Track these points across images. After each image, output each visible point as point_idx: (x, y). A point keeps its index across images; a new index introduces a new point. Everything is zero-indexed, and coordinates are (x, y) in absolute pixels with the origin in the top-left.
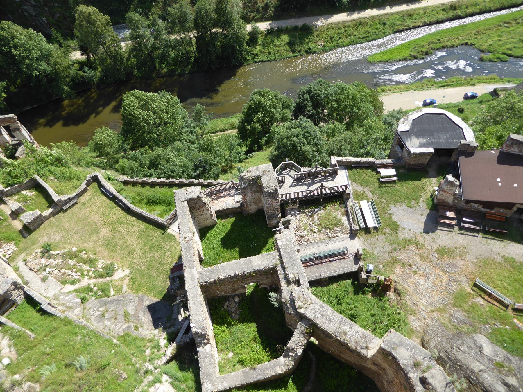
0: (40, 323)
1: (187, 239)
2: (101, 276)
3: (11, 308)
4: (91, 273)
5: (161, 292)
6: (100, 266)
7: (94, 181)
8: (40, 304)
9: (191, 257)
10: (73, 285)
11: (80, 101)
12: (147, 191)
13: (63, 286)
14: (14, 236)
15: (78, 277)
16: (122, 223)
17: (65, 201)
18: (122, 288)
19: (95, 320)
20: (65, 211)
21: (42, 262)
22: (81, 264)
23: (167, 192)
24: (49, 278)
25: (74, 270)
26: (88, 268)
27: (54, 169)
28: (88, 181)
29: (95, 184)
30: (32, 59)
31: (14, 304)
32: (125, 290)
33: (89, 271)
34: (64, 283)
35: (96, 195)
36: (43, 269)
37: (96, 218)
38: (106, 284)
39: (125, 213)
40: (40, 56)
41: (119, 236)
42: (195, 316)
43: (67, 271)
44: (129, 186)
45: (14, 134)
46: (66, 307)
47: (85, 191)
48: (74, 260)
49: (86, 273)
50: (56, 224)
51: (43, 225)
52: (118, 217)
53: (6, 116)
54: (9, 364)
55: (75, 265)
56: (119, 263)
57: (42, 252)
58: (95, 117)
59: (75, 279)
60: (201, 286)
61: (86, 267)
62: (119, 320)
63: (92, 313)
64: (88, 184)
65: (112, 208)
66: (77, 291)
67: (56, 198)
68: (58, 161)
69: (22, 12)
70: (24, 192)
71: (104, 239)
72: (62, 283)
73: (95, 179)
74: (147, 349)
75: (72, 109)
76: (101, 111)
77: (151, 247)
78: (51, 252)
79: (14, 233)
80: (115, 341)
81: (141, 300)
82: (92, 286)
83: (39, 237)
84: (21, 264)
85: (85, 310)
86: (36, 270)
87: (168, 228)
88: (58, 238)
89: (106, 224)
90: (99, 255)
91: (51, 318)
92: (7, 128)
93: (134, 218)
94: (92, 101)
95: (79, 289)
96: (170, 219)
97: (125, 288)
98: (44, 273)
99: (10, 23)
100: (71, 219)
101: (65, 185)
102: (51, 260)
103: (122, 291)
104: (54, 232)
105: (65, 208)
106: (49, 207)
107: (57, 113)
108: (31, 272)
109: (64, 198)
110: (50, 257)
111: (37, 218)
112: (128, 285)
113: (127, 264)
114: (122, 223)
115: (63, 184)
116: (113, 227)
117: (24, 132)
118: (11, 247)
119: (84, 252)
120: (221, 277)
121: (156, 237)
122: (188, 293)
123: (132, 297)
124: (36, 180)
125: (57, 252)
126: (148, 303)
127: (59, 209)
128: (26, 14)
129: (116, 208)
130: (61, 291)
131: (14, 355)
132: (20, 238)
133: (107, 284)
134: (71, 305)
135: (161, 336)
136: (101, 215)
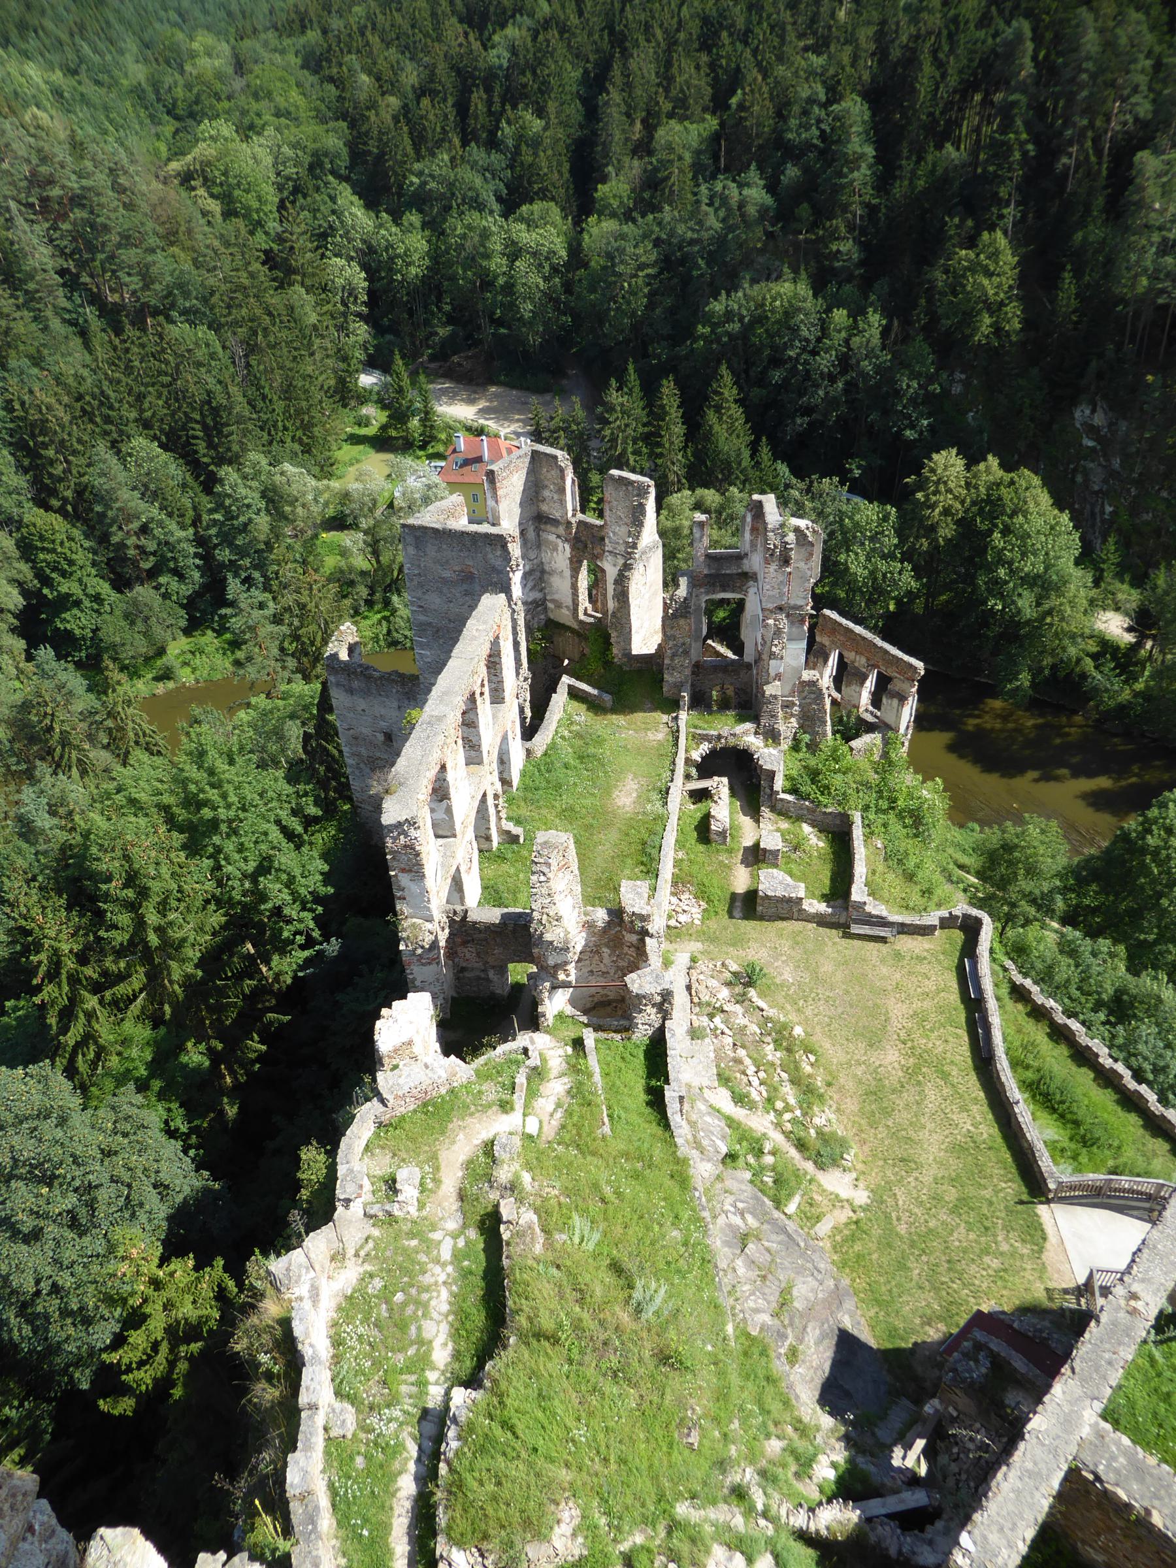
0: (635, 1118)
1: (1139, 1305)
2: (801, 1146)
3: (615, 1031)
4: (787, 1116)
5: (892, 1333)
6: (817, 1121)
7: (961, 928)
8: (667, 1082)
9: (1110, 1363)
10: (736, 1103)
11: (1030, 723)
12: (1055, 1059)
13: (716, 1084)
14: (716, 892)
15: (758, 1098)
16: (945, 1076)
17: (870, 915)
18: (818, 1219)
19: (722, 1229)
20: (848, 935)
21: (720, 996)
22: (785, 1076)
23: (1105, 1109)
24: (707, 1040)
25: (762, 1074)
26: (792, 1101)
27: (896, 827)
28: (952, 917)
29: (958, 936)
30: (1012, 572)
31: (627, 1029)
32: (821, 1234)
33: (788, 1108)
34: (724, 1079)
35: (939, 962)
36: (710, 1010)
37: (898, 1012)
38: (798, 1174)
39: (969, 1061)
40: (1038, 576)
41: (911, 1099)
42: (995, 1528)
43: (747, 1061)
44: (1020, 1006)
45: (884, 700)
46: (694, 1136)
47: (925, 931)
48: (778, 1054)
49: (779, 1105)
50: (810, 946)
51: (785, 924)
52: (948, 1055)
53: (906, 658)
54: (530, 1137)
55: (773, 1064)
56: (861, 1157)
57: (735, 974)
58: (1036, 781)
59: (747, 1095)
60: (1073, 1476)
61: (789, 1093)
62: (767, 1291)
63: (727, 1207)
64: (947, 923)
65: (951, 1021)
66: (731, 1122)
67: (858, 893)
68: (915, 820)
69: (1075, 471)
70: (806, 829)
71: (875, 1071)
72: (719, 1075)
73: (971, 928)
74: (778, 1437)
75: (998, 726)
76: (1057, 779)
77: (963, 1201)
78: (752, 993)
79: (721, 888)
80: (730, 1329)
81: (837, 1297)
82: (767, 1147)
83: (756, 941)
84: (682, 959)
85: (719, 1186)
86: (696, 1000)
87: (1048, 1202)
88: (788, 975)
89: (909, 1044)
90: (836, 1097)
91: (659, 1131)
92: (883, 683)
93: (982, 1094)
94: (1058, 741)
95: (739, 1124)
96: (1072, 1188)
97: (824, 1228)
98: (705, 1020)
99: (1036, 481)
100: (846, 963)
101: (893, 881)
102: (738, 1009)
103: (813, 1226)
104: (790, 957)
105: (856, 929)
106: (826, 898)
107: (958, 712)
108: (686, 993)
109: (875, 908)
110: (741, 999)
111: (789, 900)
112: (836, 1229)
113: (874, 1178)
114: (945, 1076)
115: (891, 876)
116: (917, 1067)
117: (907, 713)
118: (694, 910)
119: (812, 1058)
120: (1157, 1519)
121: (996, 1192)
122: (1022, 1446)
123: (822, 1266)
124: (849, 824)
125: (761, 1004)
126: (847, 1323)
127: (842, 921)
128: (1079, 479)
129: (959, 1031)
130: (705, 1090)
131: (550, 1132)
132: (723, 908)
133: (797, 1176)
134: (705, 1142)
135: (833, 1449)
136: (915, 1014)
